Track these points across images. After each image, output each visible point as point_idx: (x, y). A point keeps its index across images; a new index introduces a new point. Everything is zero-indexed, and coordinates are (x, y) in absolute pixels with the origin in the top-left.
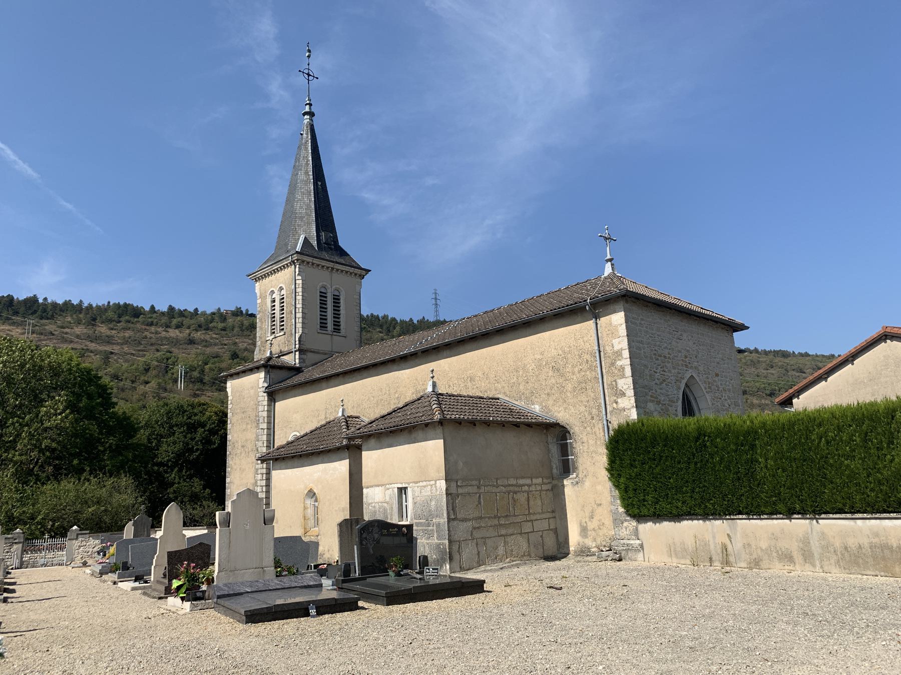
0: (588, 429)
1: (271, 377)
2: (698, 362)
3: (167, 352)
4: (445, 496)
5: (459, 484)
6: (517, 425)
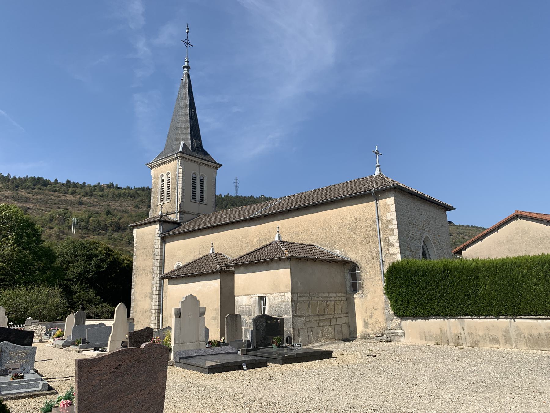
0: (370, 265)
1: (163, 228)
2: (429, 228)
3: (65, 209)
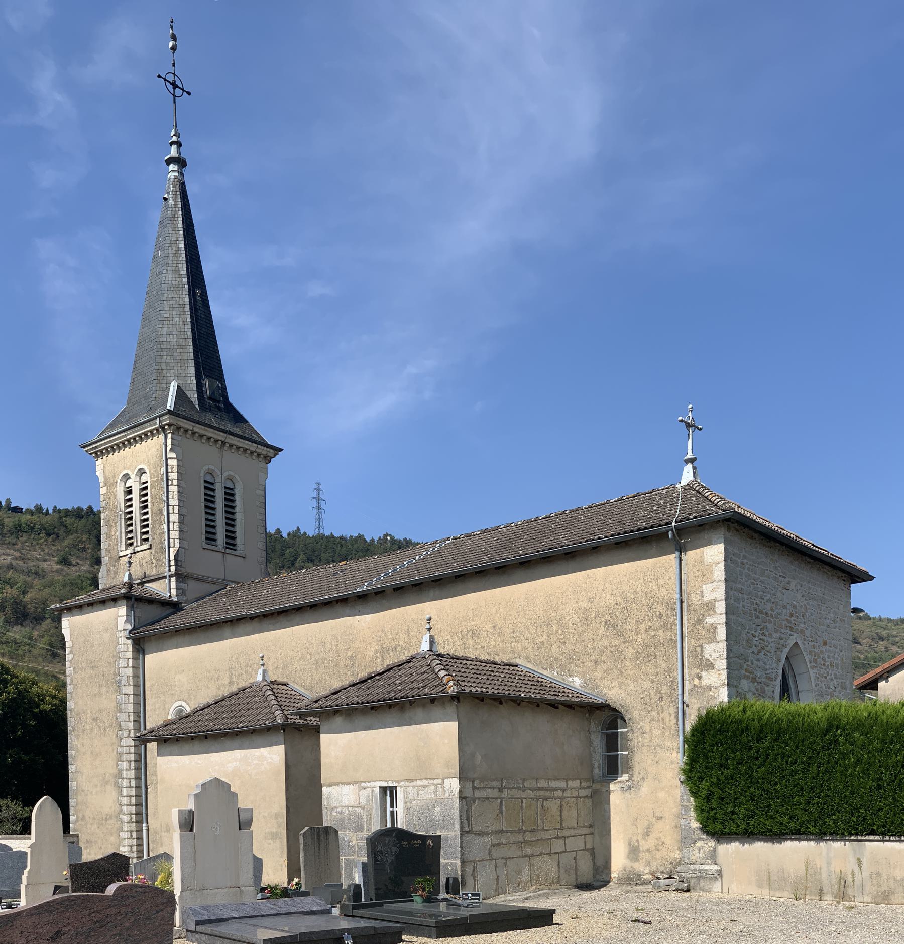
0: (654, 713)
2: (804, 623)
4: (458, 800)
5: (475, 785)
6: (554, 705)
